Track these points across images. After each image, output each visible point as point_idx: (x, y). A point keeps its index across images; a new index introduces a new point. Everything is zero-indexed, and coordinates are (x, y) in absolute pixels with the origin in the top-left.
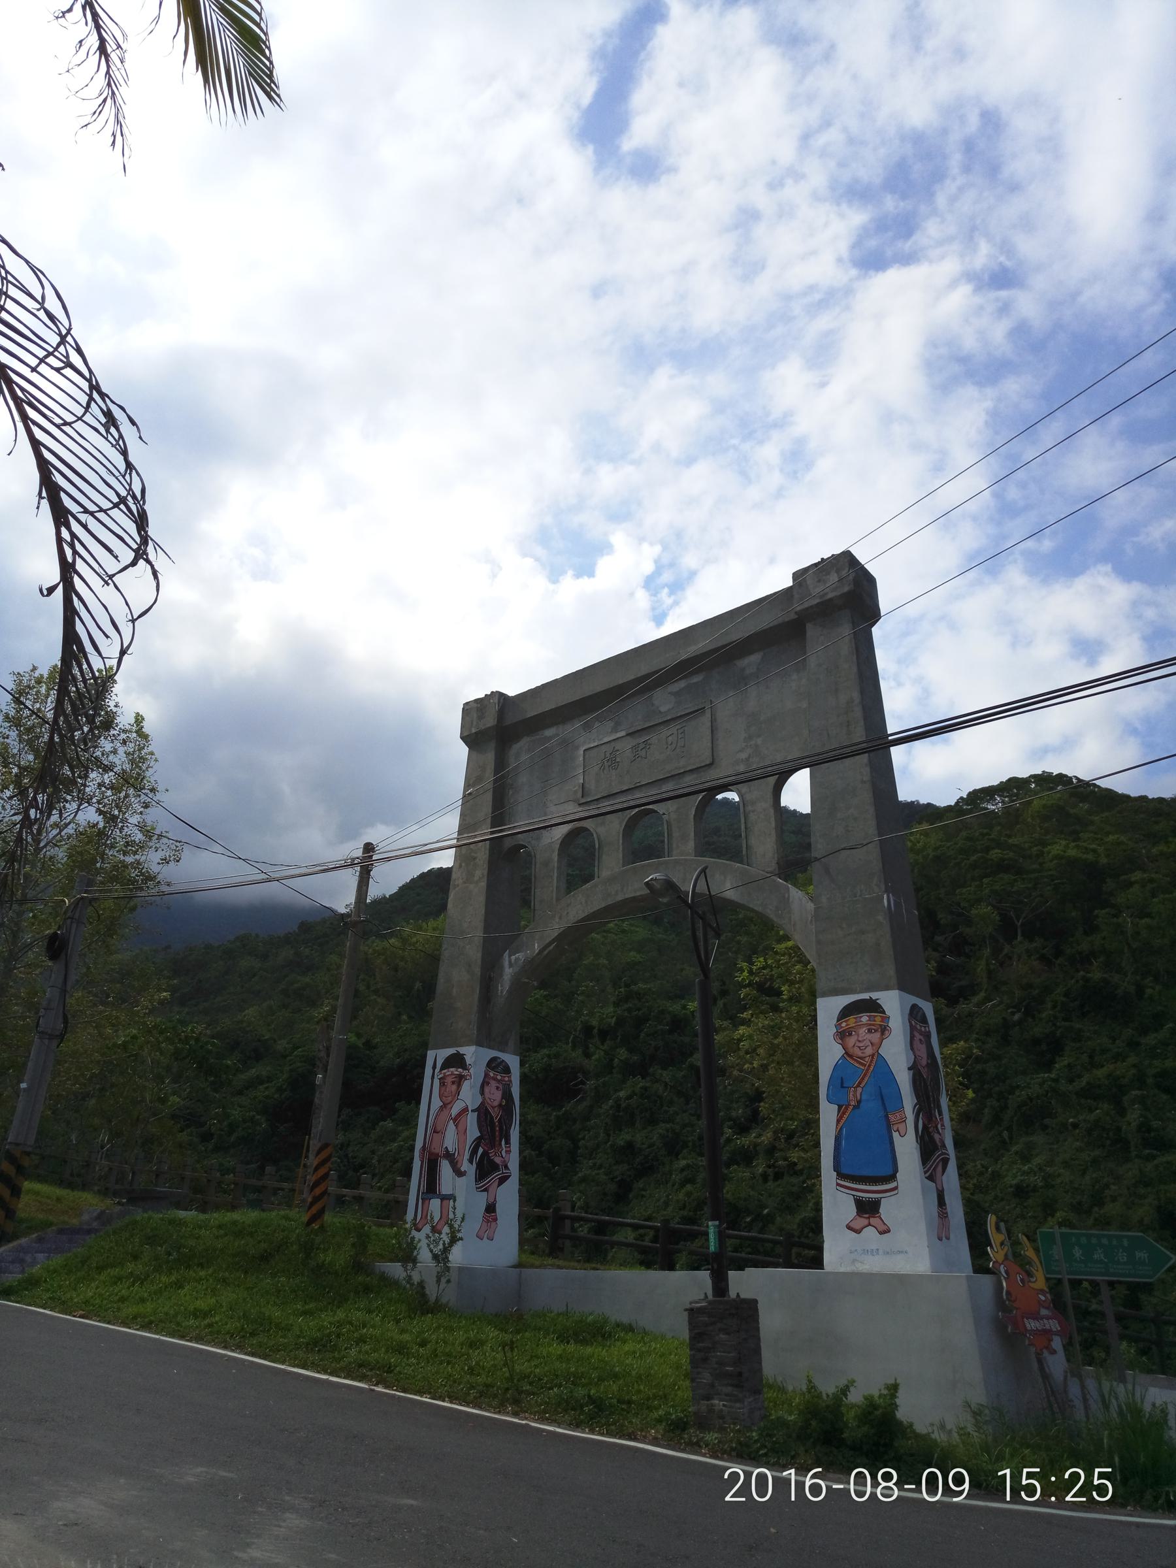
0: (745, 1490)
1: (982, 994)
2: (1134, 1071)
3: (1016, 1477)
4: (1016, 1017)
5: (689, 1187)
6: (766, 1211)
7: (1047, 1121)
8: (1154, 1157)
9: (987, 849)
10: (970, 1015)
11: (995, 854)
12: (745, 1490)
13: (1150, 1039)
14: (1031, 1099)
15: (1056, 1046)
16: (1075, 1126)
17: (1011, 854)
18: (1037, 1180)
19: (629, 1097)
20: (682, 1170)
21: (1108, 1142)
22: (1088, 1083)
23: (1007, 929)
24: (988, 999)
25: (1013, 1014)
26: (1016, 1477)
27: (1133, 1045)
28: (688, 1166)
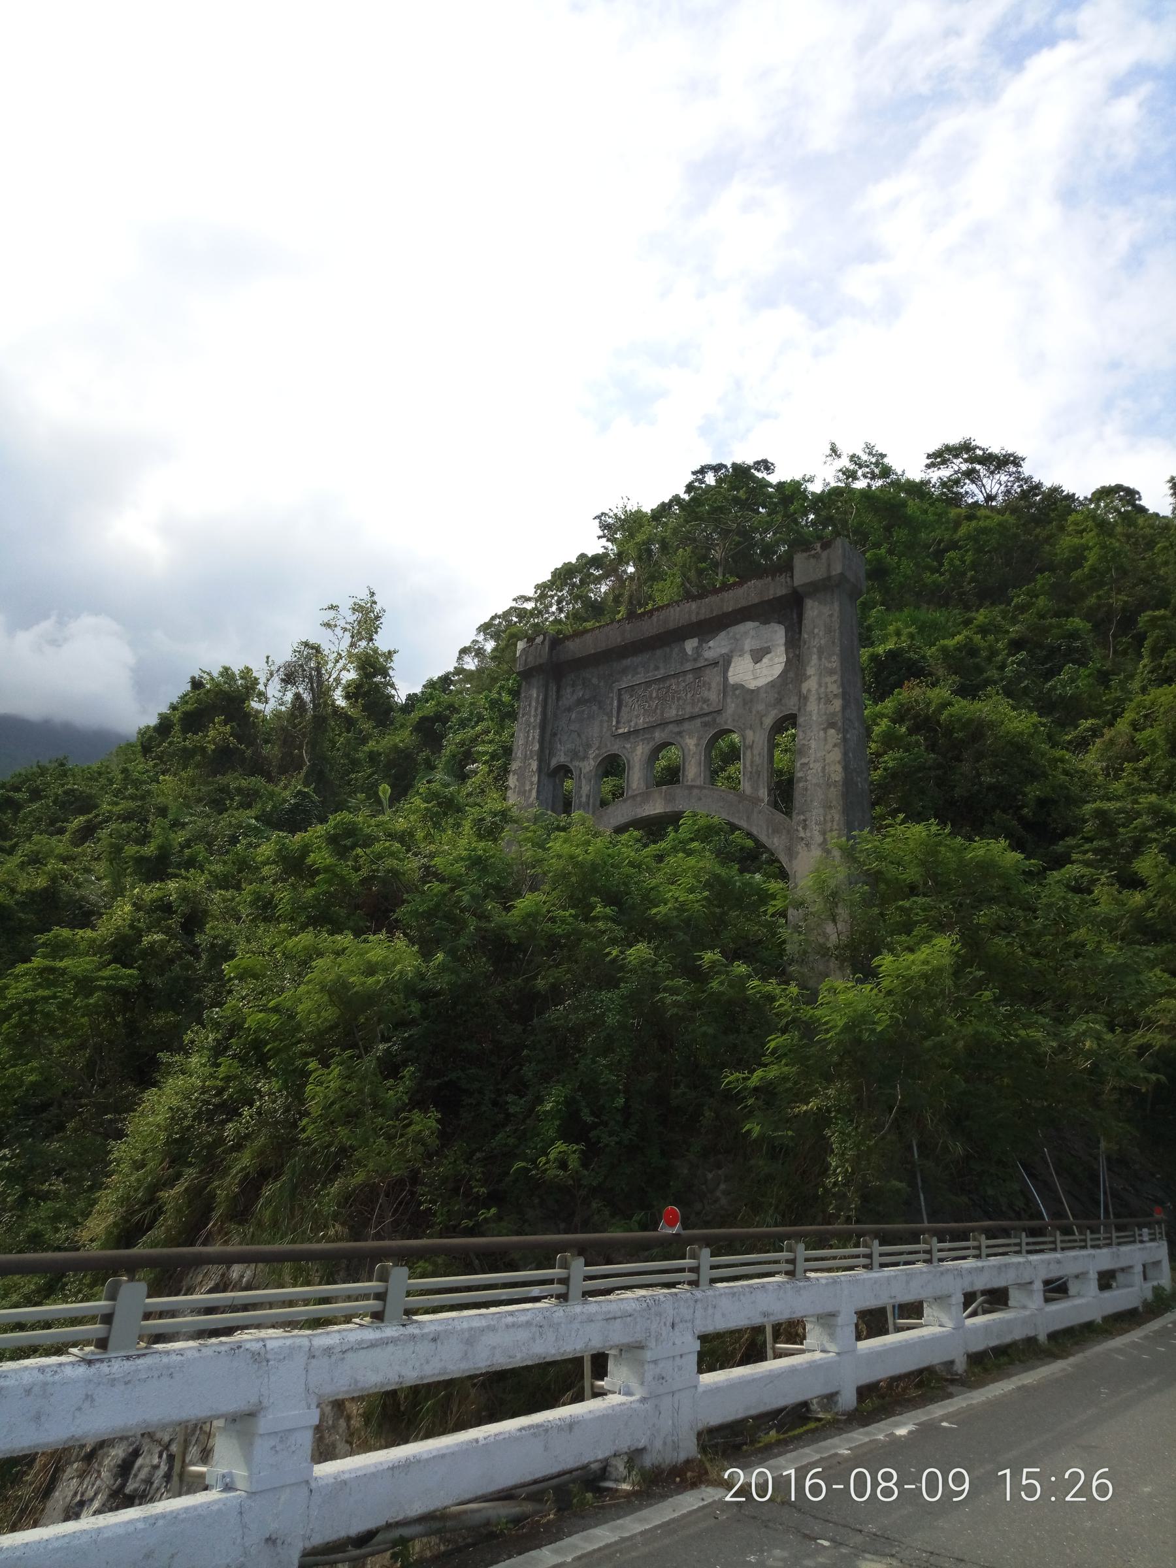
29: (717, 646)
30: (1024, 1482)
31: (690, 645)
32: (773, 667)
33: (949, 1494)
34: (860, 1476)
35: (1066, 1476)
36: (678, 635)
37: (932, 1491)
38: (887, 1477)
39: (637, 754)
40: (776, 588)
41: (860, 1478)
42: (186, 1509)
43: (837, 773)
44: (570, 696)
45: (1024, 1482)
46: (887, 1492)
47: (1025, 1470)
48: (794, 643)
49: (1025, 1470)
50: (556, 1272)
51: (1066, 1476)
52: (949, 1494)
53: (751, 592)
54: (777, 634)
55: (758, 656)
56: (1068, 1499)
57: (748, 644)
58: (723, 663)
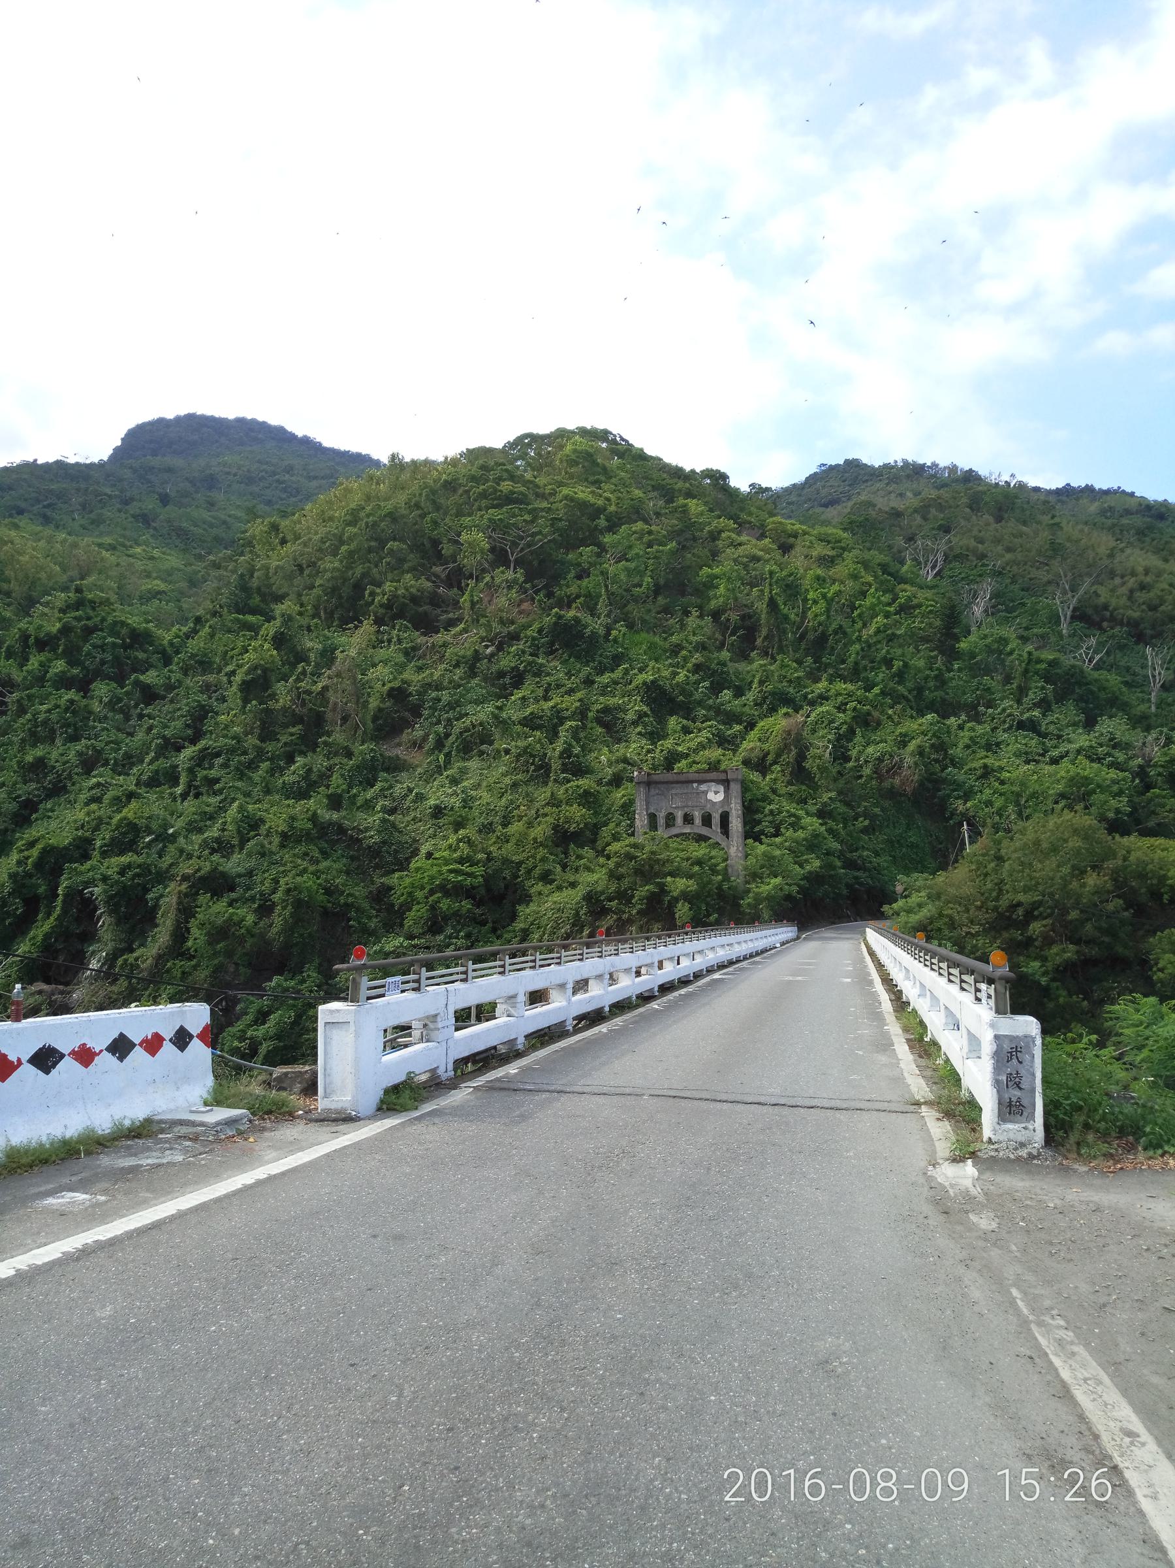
0: (743, 1491)
1: (462, 626)
2: (578, 704)
3: (1015, 1477)
4: (488, 651)
5: (94, 806)
6: (171, 831)
7: (484, 747)
8: (569, 781)
9: (499, 480)
10: (445, 645)
11: (506, 486)
12: (743, 1491)
13: (605, 678)
14: (474, 726)
15: (518, 679)
16: (507, 752)
17: (523, 489)
18: (456, 802)
19: (49, 711)
20: (92, 788)
21: (533, 768)
22: (532, 713)
23: (499, 557)
24: (465, 631)
25: (487, 647)
26: (1015, 1477)
27: (588, 682)
28: (98, 785)
29: (703, 787)
30: (1023, 1482)
31: (695, 785)
32: (720, 797)
33: (948, 1493)
34: (859, 1476)
35: (1066, 1476)
36: (693, 782)
37: (931, 1492)
38: (887, 1477)
39: (679, 815)
40: (723, 776)
41: (859, 1477)
42: (144, 1204)
43: (740, 829)
44: (653, 792)
45: (1023, 1482)
46: (887, 1492)
47: (1024, 1470)
48: (727, 791)
49: (1024, 1470)
50: (555, 955)
51: (1066, 1476)
52: (948, 1493)
53: (714, 775)
54: (721, 788)
55: (716, 793)
56: (1067, 1498)
57: (713, 789)
58: (706, 793)
